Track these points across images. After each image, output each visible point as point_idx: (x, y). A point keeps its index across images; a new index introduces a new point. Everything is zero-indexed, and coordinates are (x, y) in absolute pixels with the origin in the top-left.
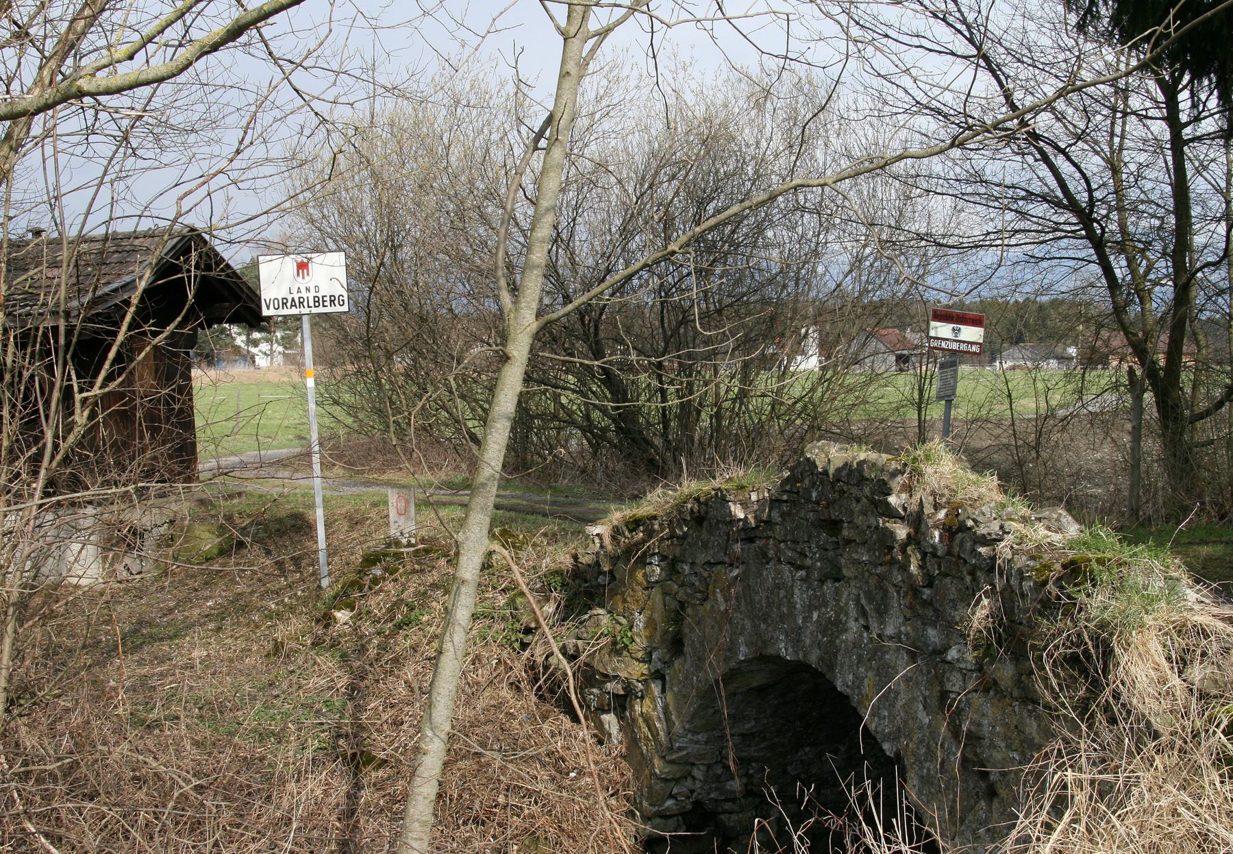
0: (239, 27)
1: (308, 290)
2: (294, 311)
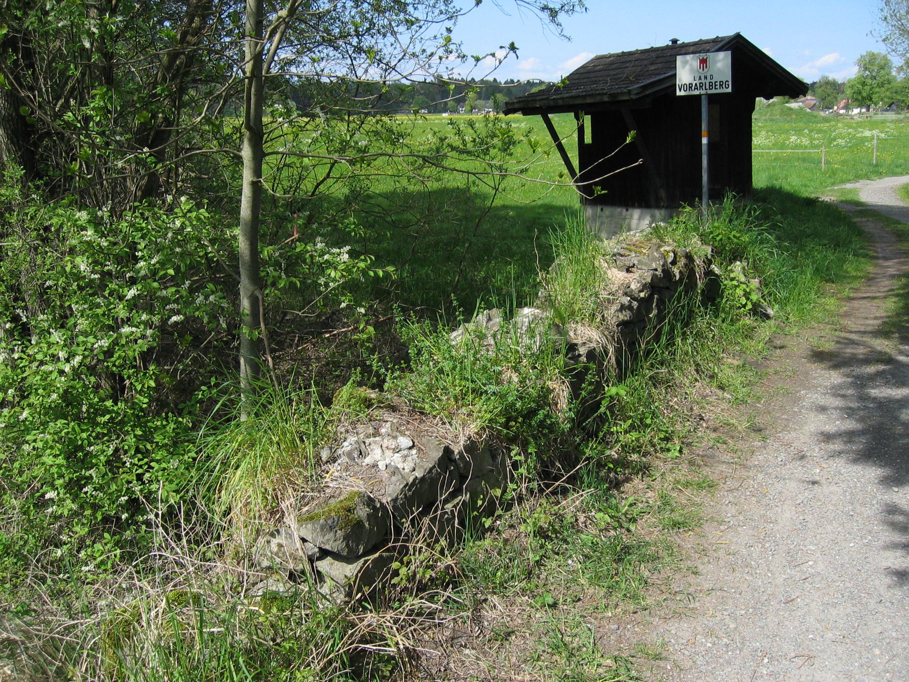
0: (251, 228)
1: (706, 78)
2: (696, 92)
